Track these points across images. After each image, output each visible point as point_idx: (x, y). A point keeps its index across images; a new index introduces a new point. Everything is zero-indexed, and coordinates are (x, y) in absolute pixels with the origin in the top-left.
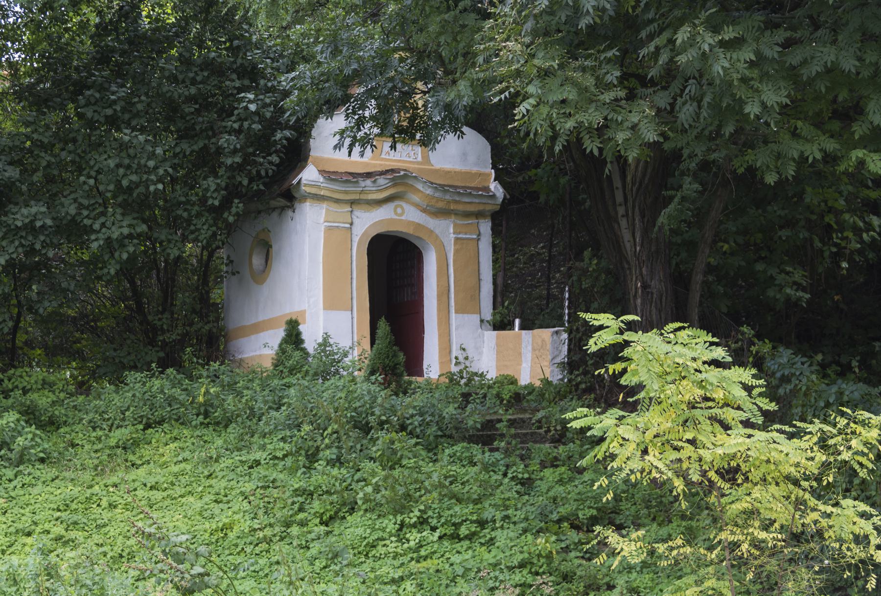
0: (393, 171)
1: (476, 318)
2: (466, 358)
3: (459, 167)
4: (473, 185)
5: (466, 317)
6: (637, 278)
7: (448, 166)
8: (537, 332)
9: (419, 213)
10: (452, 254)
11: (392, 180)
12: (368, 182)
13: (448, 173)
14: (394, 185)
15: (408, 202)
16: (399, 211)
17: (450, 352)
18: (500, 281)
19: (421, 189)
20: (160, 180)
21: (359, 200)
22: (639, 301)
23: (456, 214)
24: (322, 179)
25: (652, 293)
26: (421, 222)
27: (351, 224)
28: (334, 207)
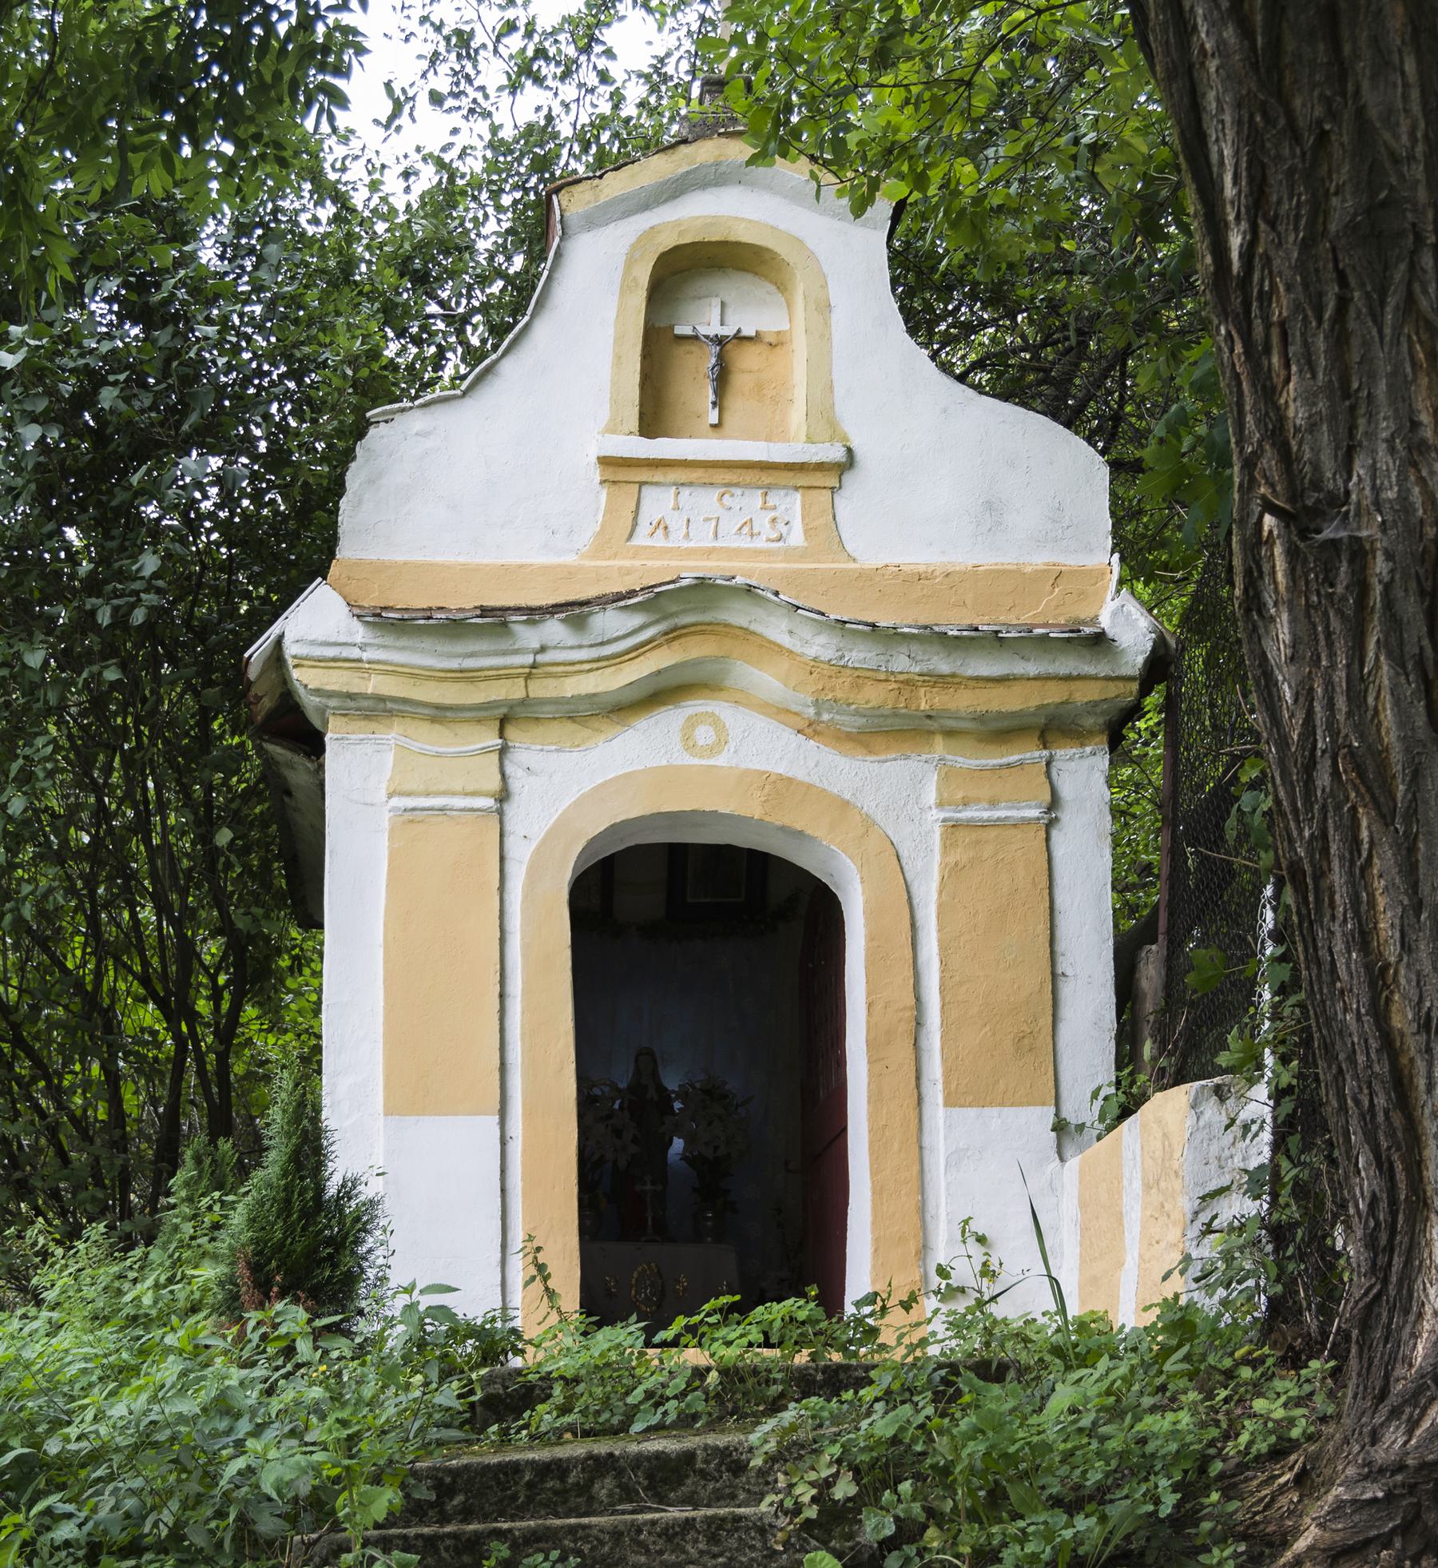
1: (1039, 1119)
2: (987, 1272)
5: (996, 1118)
9: (789, 739)
10: (935, 885)
12: (554, 630)
14: (673, 635)
15: (744, 699)
16: (704, 735)
17: (924, 1249)
18: (1150, 974)
19: (785, 640)
21: (525, 702)
22: (1281, 633)
23: (949, 733)
24: (359, 632)
25: (1359, 552)
26: (800, 775)
27: (503, 796)
28: (427, 738)
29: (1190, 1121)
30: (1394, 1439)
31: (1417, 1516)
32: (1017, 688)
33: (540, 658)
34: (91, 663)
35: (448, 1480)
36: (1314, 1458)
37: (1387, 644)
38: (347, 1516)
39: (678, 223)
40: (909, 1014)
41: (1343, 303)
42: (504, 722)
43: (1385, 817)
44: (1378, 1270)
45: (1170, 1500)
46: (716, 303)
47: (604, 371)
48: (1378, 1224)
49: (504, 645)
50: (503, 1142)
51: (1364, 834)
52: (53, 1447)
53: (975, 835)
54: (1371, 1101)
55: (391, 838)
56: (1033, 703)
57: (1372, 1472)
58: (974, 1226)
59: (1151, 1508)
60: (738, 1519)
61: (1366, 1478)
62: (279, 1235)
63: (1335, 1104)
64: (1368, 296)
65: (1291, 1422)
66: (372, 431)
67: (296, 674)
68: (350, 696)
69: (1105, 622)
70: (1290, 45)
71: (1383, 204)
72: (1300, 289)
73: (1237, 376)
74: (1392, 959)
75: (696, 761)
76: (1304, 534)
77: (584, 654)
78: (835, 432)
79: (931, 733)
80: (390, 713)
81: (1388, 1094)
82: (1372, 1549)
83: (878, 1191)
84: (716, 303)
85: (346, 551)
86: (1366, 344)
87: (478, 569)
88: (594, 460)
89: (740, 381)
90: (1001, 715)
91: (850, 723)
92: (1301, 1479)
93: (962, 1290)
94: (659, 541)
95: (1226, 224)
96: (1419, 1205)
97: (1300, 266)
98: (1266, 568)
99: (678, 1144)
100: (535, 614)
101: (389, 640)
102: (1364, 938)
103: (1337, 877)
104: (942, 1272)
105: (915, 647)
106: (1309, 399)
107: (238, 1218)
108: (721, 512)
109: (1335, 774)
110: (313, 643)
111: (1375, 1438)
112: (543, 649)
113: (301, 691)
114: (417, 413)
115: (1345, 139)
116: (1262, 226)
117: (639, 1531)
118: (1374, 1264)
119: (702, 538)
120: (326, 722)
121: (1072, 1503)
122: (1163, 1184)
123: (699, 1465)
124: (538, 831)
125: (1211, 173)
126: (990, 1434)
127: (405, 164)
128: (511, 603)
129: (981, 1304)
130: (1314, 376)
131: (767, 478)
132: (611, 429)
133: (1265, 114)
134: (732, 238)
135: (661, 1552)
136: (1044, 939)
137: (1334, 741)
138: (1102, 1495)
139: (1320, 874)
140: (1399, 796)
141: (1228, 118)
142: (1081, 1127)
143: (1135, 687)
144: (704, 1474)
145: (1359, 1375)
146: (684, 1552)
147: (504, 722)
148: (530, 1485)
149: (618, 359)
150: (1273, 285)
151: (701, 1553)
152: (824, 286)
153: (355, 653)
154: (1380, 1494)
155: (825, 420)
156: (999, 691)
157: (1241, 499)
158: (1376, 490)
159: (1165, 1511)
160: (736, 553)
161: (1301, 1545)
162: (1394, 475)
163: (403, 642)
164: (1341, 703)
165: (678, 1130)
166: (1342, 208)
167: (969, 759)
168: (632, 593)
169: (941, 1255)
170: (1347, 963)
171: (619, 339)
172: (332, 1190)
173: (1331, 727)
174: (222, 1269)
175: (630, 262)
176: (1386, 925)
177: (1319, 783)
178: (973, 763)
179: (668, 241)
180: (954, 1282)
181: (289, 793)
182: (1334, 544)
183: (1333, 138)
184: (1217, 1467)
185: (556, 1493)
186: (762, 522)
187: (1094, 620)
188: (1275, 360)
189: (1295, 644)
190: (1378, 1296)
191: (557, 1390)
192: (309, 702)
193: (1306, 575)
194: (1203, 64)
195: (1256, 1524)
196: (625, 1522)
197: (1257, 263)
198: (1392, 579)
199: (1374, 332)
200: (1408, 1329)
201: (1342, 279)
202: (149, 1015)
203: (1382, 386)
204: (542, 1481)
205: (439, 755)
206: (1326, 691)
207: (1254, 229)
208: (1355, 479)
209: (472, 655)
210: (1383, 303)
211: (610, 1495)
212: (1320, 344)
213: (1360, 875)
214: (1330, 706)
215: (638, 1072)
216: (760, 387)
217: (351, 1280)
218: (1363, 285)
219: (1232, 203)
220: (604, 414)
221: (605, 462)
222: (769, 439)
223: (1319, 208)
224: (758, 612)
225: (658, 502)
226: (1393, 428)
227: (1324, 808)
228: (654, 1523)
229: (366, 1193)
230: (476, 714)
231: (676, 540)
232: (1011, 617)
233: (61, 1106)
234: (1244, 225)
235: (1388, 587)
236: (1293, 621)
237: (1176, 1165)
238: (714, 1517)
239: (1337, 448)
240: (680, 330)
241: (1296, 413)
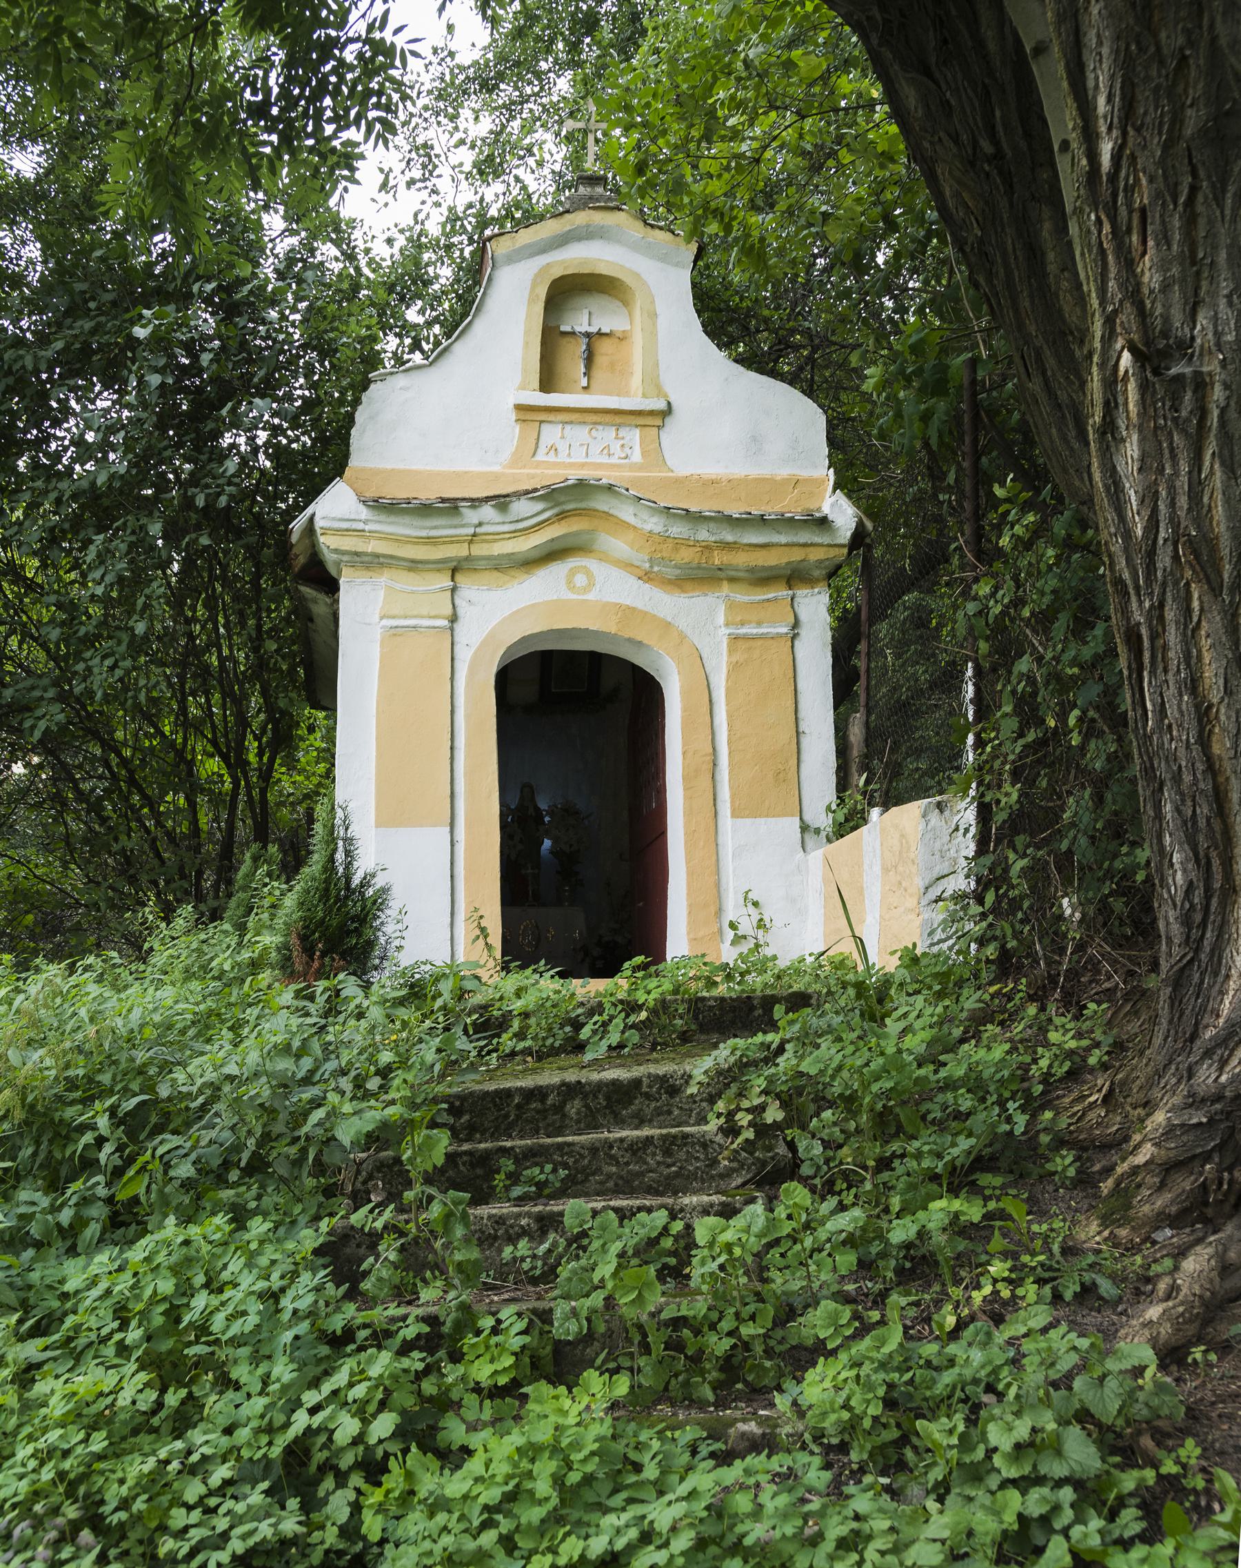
2: (761, 924)
3: (740, 469)
5: (764, 825)
7: (710, 470)
8: (762, 820)
12: (488, 512)
14: (562, 516)
15: (605, 558)
16: (580, 580)
17: (720, 911)
18: (856, 733)
21: (468, 559)
22: (1132, 448)
23: (732, 580)
24: (364, 513)
25: (1201, 384)
27: (454, 619)
30: (1206, 1076)
31: (1232, 1135)
32: (774, 551)
33: (479, 530)
34: (188, 533)
35: (457, 1103)
37: (1221, 457)
38: (409, 1159)
39: (563, 262)
41: (1194, 190)
42: (454, 571)
44: (1193, 944)
46: (586, 312)
47: (519, 353)
48: (1192, 906)
49: (456, 521)
50: (452, 845)
51: (1196, 604)
52: (164, 1091)
54: (1194, 811)
56: (784, 560)
59: (1008, 1127)
60: (686, 1136)
61: (1191, 1106)
62: (321, 914)
63: (1151, 813)
64: (1213, 186)
66: (372, 386)
67: (322, 539)
68: (356, 554)
69: (826, 509)
71: (1227, 113)
72: (1161, 179)
73: (1102, 252)
74: (1215, 701)
75: (575, 597)
78: (660, 392)
81: (1210, 805)
82: (1197, 1163)
83: (690, 873)
84: (586, 312)
85: (355, 462)
86: (1211, 222)
87: (439, 474)
88: (511, 406)
89: (600, 360)
91: (671, 573)
93: (745, 937)
94: (551, 458)
95: (1098, 135)
96: (1229, 890)
97: (1162, 163)
98: (1121, 400)
99: (547, 843)
100: (475, 502)
101: (383, 517)
102: (1193, 685)
103: (1172, 636)
104: (733, 926)
105: (712, 525)
106: (1163, 266)
107: (290, 901)
108: (590, 440)
109: (1176, 557)
110: (334, 519)
112: (480, 524)
113: (325, 551)
114: (400, 376)
115: (1201, 62)
116: (1131, 132)
117: (611, 1147)
118: (1188, 937)
119: (579, 457)
120: (340, 572)
122: (900, 869)
123: (645, 1089)
124: (476, 641)
125: (1086, 95)
126: (894, 1073)
127: (388, 234)
129: (757, 946)
130: (1169, 248)
131: (618, 419)
132: (523, 387)
133: (1138, 44)
134: (597, 271)
135: (627, 1164)
137: (1176, 531)
140: (1226, 576)
141: (1105, 51)
143: (845, 551)
144: (648, 1096)
145: (1170, 1022)
146: (646, 1163)
147: (454, 571)
148: (518, 1106)
150: (1137, 180)
151: (658, 1163)
152: (653, 302)
153: (361, 526)
154: (1204, 1120)
155: (654, 384)
156: (763, 552)
157: (1103, 347)
158: (1218, 335)
159: (1019, 1129)
160: (600, 466)
161: (1140, 1159)
162: (1232, 323)
163: (392, 518)
164: (1183, 501)
165: (548, 834)
167: (743, 596)
168: (536, 490)
169: (730, 914)
171: (527, 333)
172: (356, 881)
173: (1174, 522)
174: (278, 939)
175: (535, 284)
177: (1159, 565)
178: (746, 598)
179: (558, 273)
180: (740, 933)
181: (311, 620)
182: (1179, 378)
183: (1191, 61)
185: (538, 1112)
186: (616, 447)
187: (819, 510)
188: (1135, 238)
189: (1142, 459)
190: (1191, 961)
191: (516, 1024)
192: (329, 558)
193: (1155, 403)
194: (1086, 9)
195: (1071, 1132)
196: (600, 1140)
197: (1124, 163)
198: (1228, 405)
199: (1218, 213)
200: (1217, 988)
201: (1194, 173)
202: (213, 765)
203: (1223, 255)
204: (528, 1103)
205: (413, 592)
206: (1169, 493)
207: (1124, 134)
208: (1199, 327)
209: (435, 528)
210: (1224, 191)
211: (578, 1113)
213: (1190, 636)
214: (1172, 504)
215: (522, 798)
216: (612, 365)
217: (371, 944)
218: (1209, 177)
219: (1105, 117)
220: (518, 379)
221: (519, 408)
223: (1177, 119)
225: (551, 433)
226: (1232, 286)
227: (1164, 585)
228: (622, 1140)
229: (379, 882)
230: (436, 565)
232: (771, 509)
233: (159, 824)
234: (1115, 133)
235: (1223, 411)
236: (1142, 441)
237: (912, 856)
238: (668, 1135)
239: (1185, 304)
240: (564, 328)
241: (1150, 278)
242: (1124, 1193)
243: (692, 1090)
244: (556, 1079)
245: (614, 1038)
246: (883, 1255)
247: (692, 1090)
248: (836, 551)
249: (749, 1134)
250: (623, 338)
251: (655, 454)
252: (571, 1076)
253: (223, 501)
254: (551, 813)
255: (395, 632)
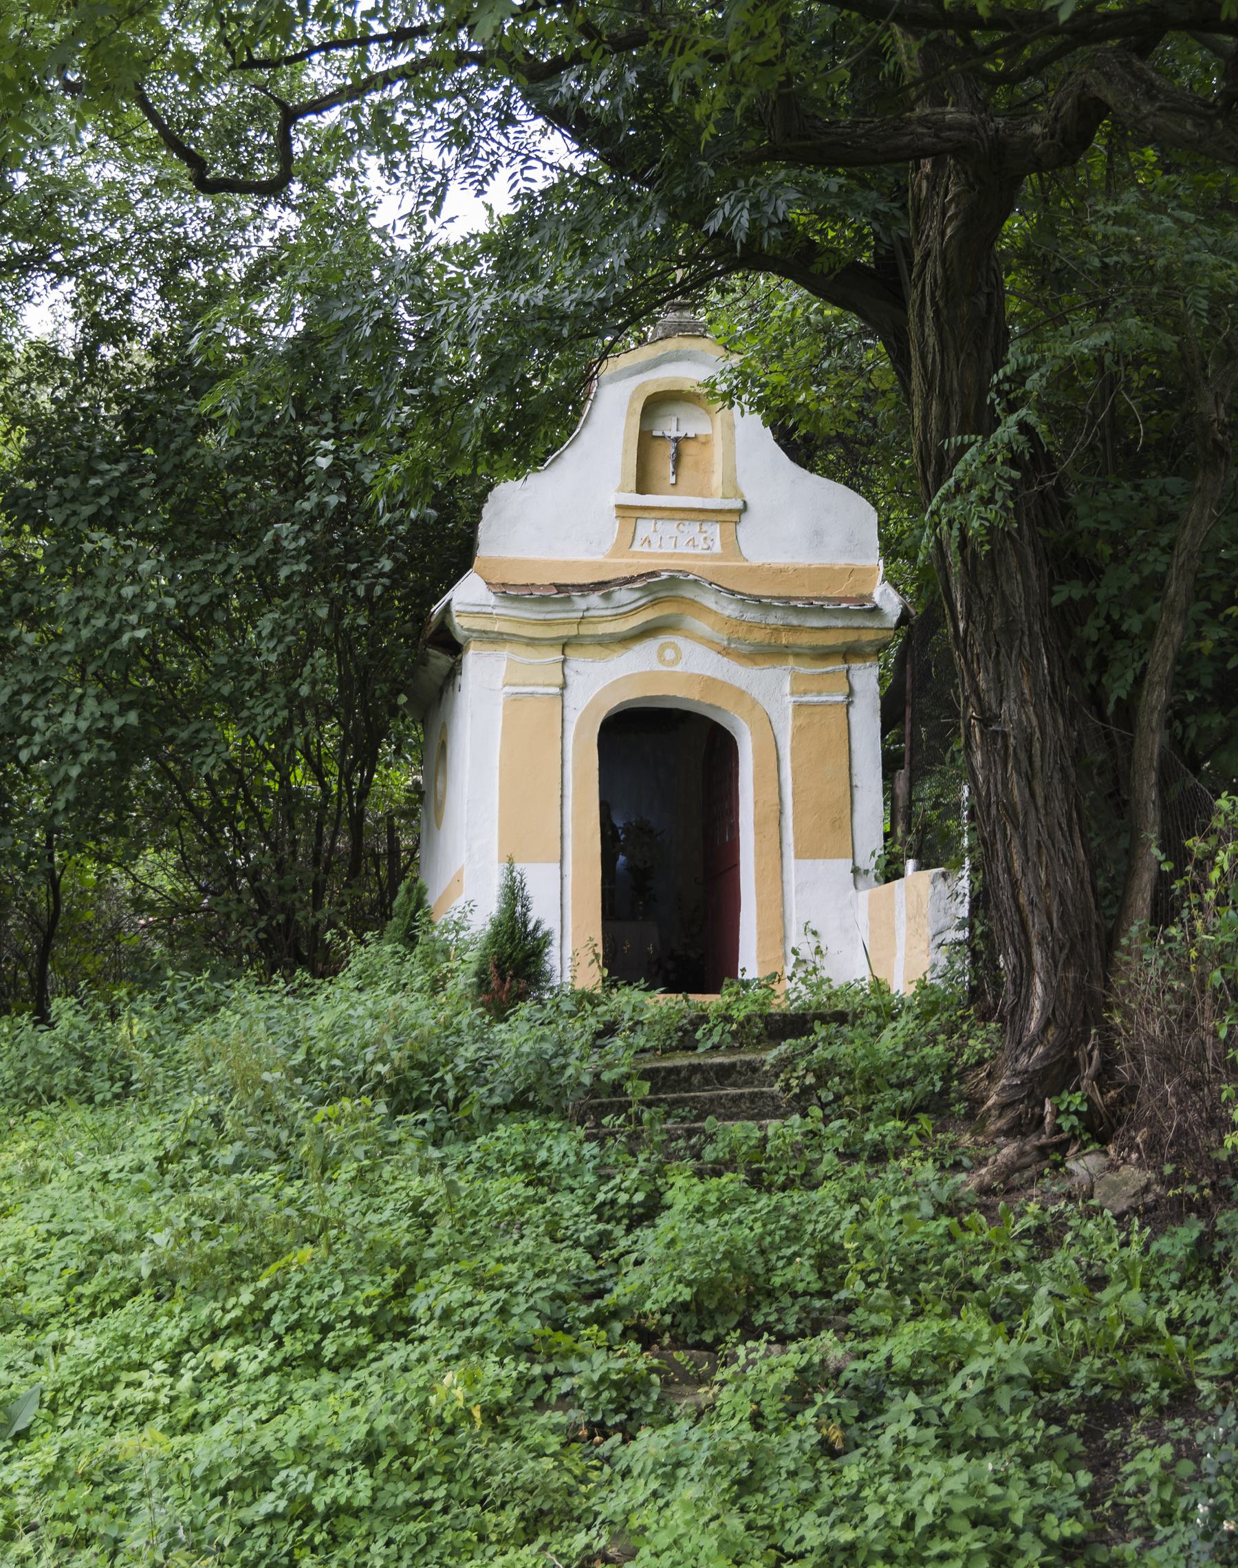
0: (653, 574)
1: (846, 865)
2: (818, 951)
3: (804, 559)
4: (835, 594)
5: (821, 865)
6: (967, 699)
7: (780, 559)
8: (819, 862)
9: (713, 657)
11: (646, 589)
12: (594, 599)
13: (778, 572)
14: (655, 602)
15: (691, 636)
16: (669, 654)
17: (784, 939)
19: (713, 606)
20: (145, 620)
22: (978, 758)
23: (797, 655)
24: (493, 600)
25: (1005, 736)
26: (719, 676)
27: (564, 686)
29: (931, 891)
32: (832, 633)
36: (994, 1067)
40: (776, 808)
41: (998, 653)
42: (564, 646)
43: (1016, 828)
44: (1017, 993)
45: (939, 1085)
47: (618, 459)
49: (568, 607)
53: (810, 710)
55: (505, 708)
56: (840, 641)
57: (1016, 1074)
58: (810, 926)
65: (984, 1050)
67: (456, 620)
70: (979, 568)
76: (986, 726)
77: (608, 612)
78: (738, 494)
79: (787, 654)
80: (505, 641)
83: (760, 906)
89: (687, 461)
90: (823, 647)
91: (745, 649)
92: (989, 1075)
93: (805, 961)
94: (646, 549)
97: (984, 639)
99: (622, 859)
100: (585, 589)
101: (508, 604)
102: (1009, 870)
103: (999, 846)
104: (795, 952)
106: (987, 682)
111: (1017, 1060)
121: (901, 1086)
128: (569, 582)
131: (702, 516)
132: (621, 489)
136: (846, 768)
138: (911, 1083)
139: (994, 844)
142: (867, 872)
144: (740, 1073)
147: (564, 646)
149: (625, 451)
153: (489, 610)
156: (823, 634)
159: (937, 1089)
161: (990, 1103)
165: (623, 851)
166: (997, 622)
167: (807, 669)
170: (1004, 878)
171: (626, 441)
176: (1017, 865)
178: (809, 671)
179: (652, 390)
181: (425, 664)
184: (955, 1070)
186: (700, 539)
187: (869, 598)
212: (991, 665)
213: (1007, 847)
220: (618, 481)
221: (619, 507)
222: (701, 495)
223: (989, 621)
224: (698, 591)
225: (645, 528)
229: (545, 927)
230: (551, 642)
231: (655, 549)
240: (655, 433)
241: (983, 685)
242: (984, 1119)
243: (767, 1067)
244: (685, 1062)
245: (715, 1039)
246: (862, 1150)
247: (767, 1067)
248: (885, 633)
249: (797, 1090)
250: (706, 442)
251: (732, 546)
252: (695, 1061)
253: (378, 590)
254: (626, 830)
255: (515, 698)
